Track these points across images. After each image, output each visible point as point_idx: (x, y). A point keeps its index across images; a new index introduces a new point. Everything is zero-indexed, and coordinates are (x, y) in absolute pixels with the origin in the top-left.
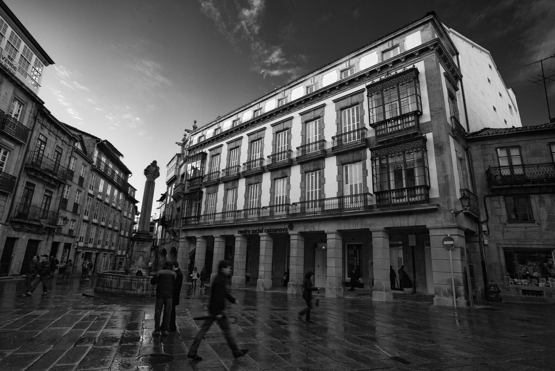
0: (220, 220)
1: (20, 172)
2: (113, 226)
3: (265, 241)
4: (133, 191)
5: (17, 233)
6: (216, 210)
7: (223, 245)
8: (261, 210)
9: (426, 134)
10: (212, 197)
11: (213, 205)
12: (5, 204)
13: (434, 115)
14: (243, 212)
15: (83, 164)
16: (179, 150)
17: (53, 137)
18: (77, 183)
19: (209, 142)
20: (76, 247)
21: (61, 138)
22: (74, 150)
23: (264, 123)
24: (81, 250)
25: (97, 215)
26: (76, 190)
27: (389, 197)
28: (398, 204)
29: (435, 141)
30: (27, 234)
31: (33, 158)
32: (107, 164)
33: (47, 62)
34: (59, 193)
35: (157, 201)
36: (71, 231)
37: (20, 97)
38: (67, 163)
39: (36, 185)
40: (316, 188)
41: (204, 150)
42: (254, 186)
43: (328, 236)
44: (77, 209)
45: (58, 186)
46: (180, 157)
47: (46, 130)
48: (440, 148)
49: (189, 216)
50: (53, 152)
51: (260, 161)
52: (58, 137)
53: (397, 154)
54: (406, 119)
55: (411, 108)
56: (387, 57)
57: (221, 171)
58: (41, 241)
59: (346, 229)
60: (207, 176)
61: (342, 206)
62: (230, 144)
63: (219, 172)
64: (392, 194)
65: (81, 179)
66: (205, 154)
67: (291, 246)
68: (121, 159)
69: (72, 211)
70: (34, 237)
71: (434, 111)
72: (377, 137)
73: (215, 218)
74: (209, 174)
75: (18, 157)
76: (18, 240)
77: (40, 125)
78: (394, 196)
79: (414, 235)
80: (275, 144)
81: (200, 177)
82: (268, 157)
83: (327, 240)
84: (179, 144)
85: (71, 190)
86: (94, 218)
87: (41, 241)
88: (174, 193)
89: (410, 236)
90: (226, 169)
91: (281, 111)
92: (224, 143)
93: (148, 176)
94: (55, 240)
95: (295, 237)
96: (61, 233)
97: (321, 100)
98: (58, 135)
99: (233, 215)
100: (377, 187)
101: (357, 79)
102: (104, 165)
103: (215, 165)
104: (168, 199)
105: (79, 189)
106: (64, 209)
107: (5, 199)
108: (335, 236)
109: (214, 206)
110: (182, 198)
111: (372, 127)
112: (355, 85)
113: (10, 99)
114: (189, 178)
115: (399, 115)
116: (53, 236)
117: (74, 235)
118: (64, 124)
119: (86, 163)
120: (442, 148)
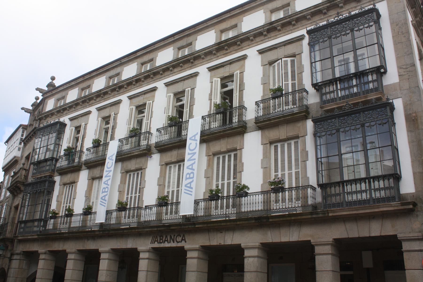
0: (78, 225)
3: (147, 260)
7: (81, 266)
8: (143, 212)
9: (394, 101)
10: (69, 192)
13: (404, 73)
19: (71, 107)
27: (341, 191)
28: (350, 202)
29: (405, 111)
40: (229, 179)
41: (62, 120)
42: (224, 158)
43: (247, 253)
46: (26, 129)
48: (413, 120)
49: (338, 179)
53: (353, 128)
54: (330, 87)
55: (376, 62)
56: (275, 17)
59: (274, 241)
61: (268, 205)
62: (102, 111)
64: (345, 187)
66: (64, 125)
67: (187, 267)
71: (403, 68)
72: (323, 103)
78: (42, 225)
79: (371, 252)
81: (52, 159)
83: (186, 259)
84: (27, 111)
88: (11, 182)
89: (364, 253)
91: (239, 43)
95: (195, 254)
97: (241, 49)
100: (322, 176)
101: (134, 83)
108: (257, 253)
111: (315, 89)
112: (289, 31)
115: (352, 70)
120: (417, 120)
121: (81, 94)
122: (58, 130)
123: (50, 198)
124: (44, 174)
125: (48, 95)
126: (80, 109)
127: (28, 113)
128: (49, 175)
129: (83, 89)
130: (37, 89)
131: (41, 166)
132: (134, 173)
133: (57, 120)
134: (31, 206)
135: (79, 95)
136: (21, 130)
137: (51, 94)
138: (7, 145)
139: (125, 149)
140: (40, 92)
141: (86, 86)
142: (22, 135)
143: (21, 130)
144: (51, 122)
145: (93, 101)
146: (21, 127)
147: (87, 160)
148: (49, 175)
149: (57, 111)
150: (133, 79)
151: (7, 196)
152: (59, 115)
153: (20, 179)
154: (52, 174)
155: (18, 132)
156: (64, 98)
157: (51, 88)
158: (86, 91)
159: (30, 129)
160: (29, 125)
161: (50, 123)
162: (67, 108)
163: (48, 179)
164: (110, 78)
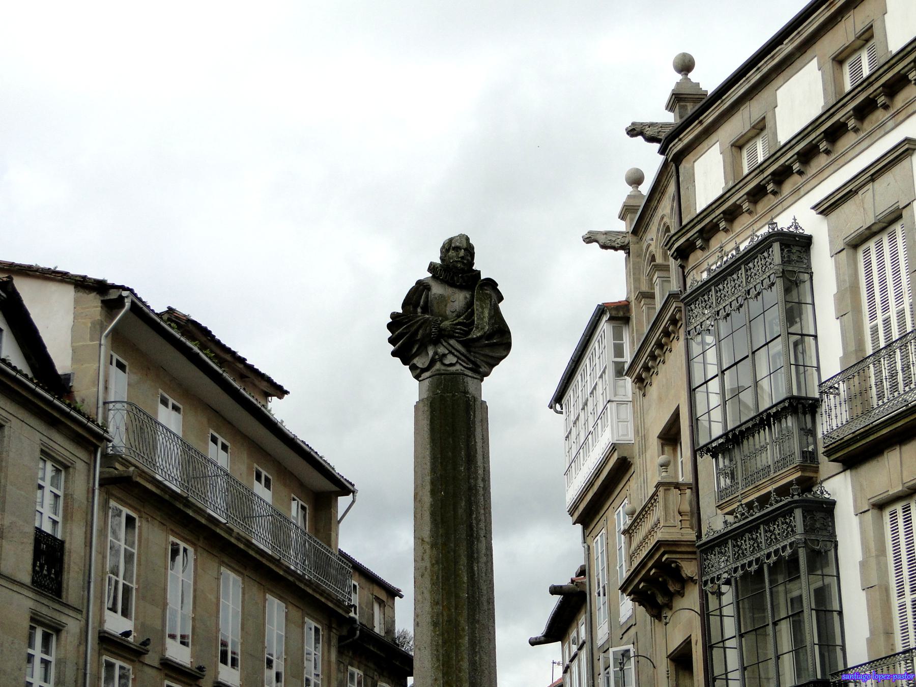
4: (381, 603)
15: (46, 455)
18: (27, 579)
26: (26, 623)
32: (193, 441)
35: (534, 642)
41: (784, 222)
60: (842, 387)
68: (276, 408)
84: (608, 242)
93: (421, 362)
102: (176, 451)
103: (885, 301)
105: (44, 611)
110: (691, 579)
119: (62, 446)
121: (838, 81)
122: (783, 272)
123: (827, 580)
124: (773, 481)
125: (686, 141)
126: (853, 147)
127: (616, 249)
128: (799, 481)
129: (739, 146)
130: (634, 131)
131: (746, 452)
132: (904, 503)
133: (765, 230)
134: (752, 636)
135: (831, 89)
136: (605, 327)
137: (700, 129)
138: (561, 413)
139: (840, 425)
140: (651, 139)
141: (852, 38)
142: (619, 351)
143: (605, 327)
144: (737, 249)
145: (795, 180)
146: (605, 318)
147: (834, 435)
148: (797, 479)
149: (748, 194)
151: (623, 620)
152: (762, 207)
153: (667, 530)
154: (808, 474)
155: (594, 344)
156: (763, 129)
157: (691, 109)
158: (859, 58)
159: (642, 319)
160: (633, 298)
161: (734, 252)
162: (768, 183)
163: (796, 497)
164: (839, 60)
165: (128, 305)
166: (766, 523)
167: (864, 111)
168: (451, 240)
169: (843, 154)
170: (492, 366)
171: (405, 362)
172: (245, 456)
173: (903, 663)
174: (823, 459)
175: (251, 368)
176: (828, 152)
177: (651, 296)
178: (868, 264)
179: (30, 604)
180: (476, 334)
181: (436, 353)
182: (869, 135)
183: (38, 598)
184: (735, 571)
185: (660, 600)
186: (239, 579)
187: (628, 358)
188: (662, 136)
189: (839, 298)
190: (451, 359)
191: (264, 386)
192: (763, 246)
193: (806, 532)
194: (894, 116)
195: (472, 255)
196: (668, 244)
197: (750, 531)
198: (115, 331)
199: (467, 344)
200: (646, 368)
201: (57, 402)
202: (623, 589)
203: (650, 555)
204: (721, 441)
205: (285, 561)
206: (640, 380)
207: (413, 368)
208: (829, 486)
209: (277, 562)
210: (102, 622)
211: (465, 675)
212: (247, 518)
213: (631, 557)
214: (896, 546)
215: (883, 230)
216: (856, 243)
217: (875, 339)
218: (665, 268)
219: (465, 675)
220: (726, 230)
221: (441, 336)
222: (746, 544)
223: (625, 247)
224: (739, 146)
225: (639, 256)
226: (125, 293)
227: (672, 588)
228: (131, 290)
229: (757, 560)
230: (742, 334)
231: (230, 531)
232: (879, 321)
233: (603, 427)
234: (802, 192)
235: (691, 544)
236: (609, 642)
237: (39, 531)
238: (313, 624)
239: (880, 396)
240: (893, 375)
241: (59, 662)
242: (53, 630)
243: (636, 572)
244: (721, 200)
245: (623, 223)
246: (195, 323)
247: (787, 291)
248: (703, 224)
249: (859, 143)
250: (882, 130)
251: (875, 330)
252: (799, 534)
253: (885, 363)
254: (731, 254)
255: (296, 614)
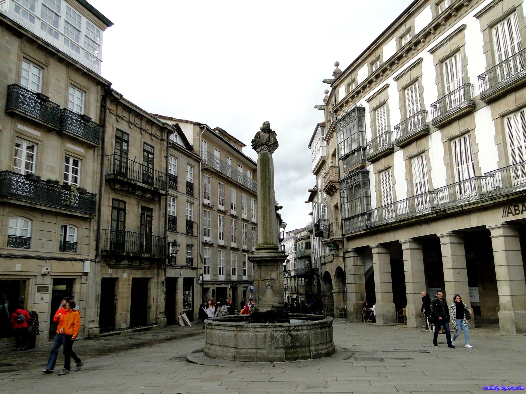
1: (101, 187)
2: (250, 246)
3: (503, 237)
5: (114, 270)
6: (395, 197)
11: (390, 190)
12: (90, 233)
14: (446, 191)
15: (188, 164)
16: (321, 117)
17: (136, 131)
18: (185, 193)
20: (200, 282)
21: (148, 131)
22: (169, 145)
23: (460, 18)
24: (208, 286)
25: (235, 236)
30: (129, 271)
31: (114, 164)
33: (103, 24)
34: (161, 209)
35: (306, 202)
36: (190, 260)
37: (77, 81)
38: (164, 165)
39: (127, 202)
41: (358, 104)
44: (192, 229)
45: (156, 198)
47: (124, 123)
50: (140, 152)
51: (464, 91)
52: (144, 130)
57: (393, 129)
58: (151, 278)
60: (372, 144)
62: (401, 80)
63: (390, 132)
65: (190, 186)
66: (362, 110)
69: (185, 232)
70: (139, 274)
73: (396, 211)
74: (375, 139)
75: (93, 166)
76: (118, 281)
77: (114, 117)
80: (489, 48)
82: (480, 77)
84: (320, 108)
85: (178, 203)
86: (220, 239)
87: (151, 278)
90: (402, 123)
92: (390, 80)
93: (258, 150)
94: (168, 275)
96: (175, 264)
98: (142, 127)
99: (428, 199)
102: (219, 162)
103: (382, 123)
104: (320, 196)
105: (190, 199)
106: (174, 229)
107: (88, 227)
109: (392, 191)
113: (64, 87)
114: (343, 154)
116: (165, 270)
117: (195, 265)
118: (157, 115)
121: (372, 69)
123: (367, 189)
124: (355, 166)
125: (337, 84)
127: (322, 110)
128: (361, 167)
132: (385, 171)
133: (354, 106)
135: (370, 71)
140: (329, 83)
142: (323, 134)
146: (319, 127)
149: (351, 97)
150: (430, 27)
151: (324, 198)
152: (354, 100)
155: (317, 133)
157: (338, 75)
159: (328, 126)
163: (360, 170)
165: (205, 128)
166: (353, 176)
167: (377, 77)
168: (265, 122)
169: (373, 87)
170: (274, 150)
171: (255, 150)
172: (236, 161)
173: (458, 185)
174: (367, 161)
175: (237, 140)
176: (369, 87)
177: (330, 121)
178: (378, 114)
179: (186, 198)
180: (270, 144)
181: (261, 148)
182: (379, 83)
183: (188, 197)
184: (347, 187)
185: (332, 193)
186: (235, 190)
187: (325, 136)
188: (331, 83)
189: (371, 123)
190: (265, 149)
191: (241, 144)
192: (353, 110)
193: (362, 178)
194: (384, 78)
195: (270, 126)
196: (333, 109)
197: (350, 178)
198: (203, 134)
199: (268, 146)
200: (329, 139)
201: (190, 152)
202: (323, 191)
203: (328, 183)
204: (344, 157)
205: (246, 186)
206: (327, 141)
207: (257, 151)
208: (368, 167)
209: (244, 186)
210: (203, 201)
211: (268, 218)
212: (237, 176)
213: (325, 184)
214: (383, 181)
215: (381, 106)
216: (375, 109)
217: (379, 133)
218: (333, 114)
219: (268, 218)
220: (346, 106)
221: (262, 145)
222: (349, 181)
223: (324, 109)
224: (349, 85)
225: (327, 111)
226: (205, 126)
227: (334, 191)
228: (206, 125)
229: (351, 185)
230: (349, 131)
231: (232, 179)
232: (380, 128)
233: (319, 152)
234: (363, 97)
235: (337, 181)
236: (322, 203)
237: (187, 181)
238: (253, 200)
239: (380, 146)
240: (383, 141)
241: (194, 211)
242: (192, 204)
243: (326, 187)
244: (344, 99)
245: (324, 103)
246: (223, 130)
247: (359, 121)
248: (340, 105)
249: (376, 85)
250: (381, 81)
251: (379, 130)
252: (360, 179)
253: (384, 137)
254: (346, 112)
255: (249, 197)
